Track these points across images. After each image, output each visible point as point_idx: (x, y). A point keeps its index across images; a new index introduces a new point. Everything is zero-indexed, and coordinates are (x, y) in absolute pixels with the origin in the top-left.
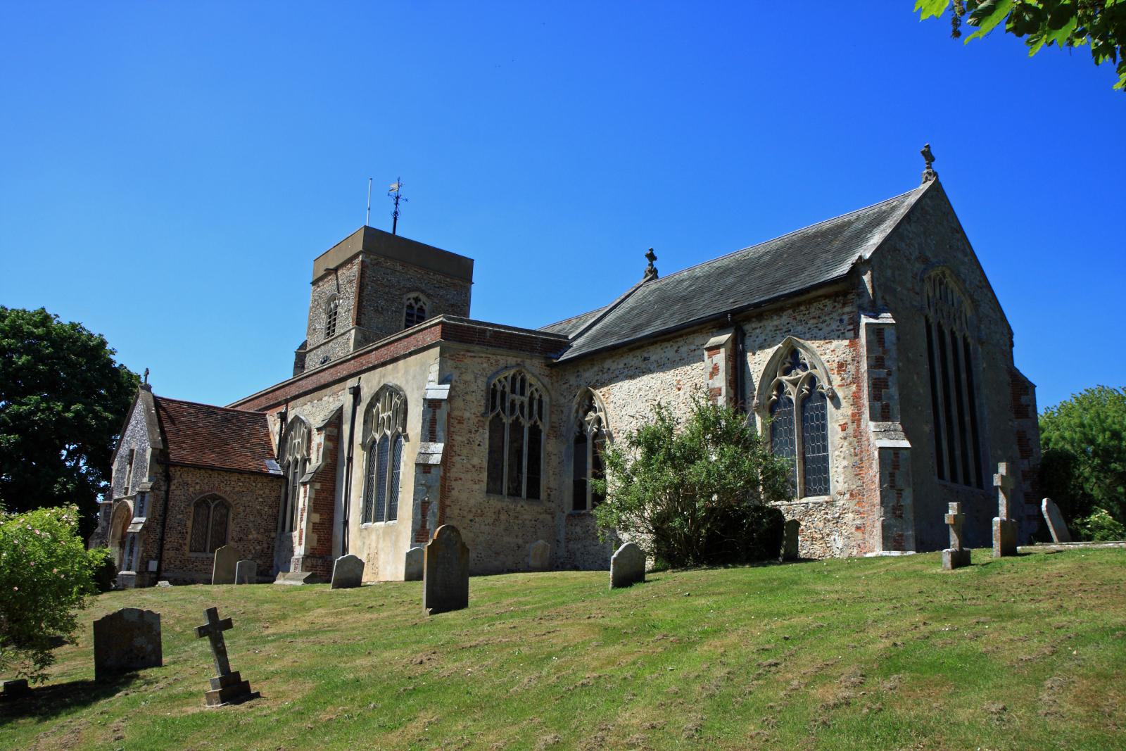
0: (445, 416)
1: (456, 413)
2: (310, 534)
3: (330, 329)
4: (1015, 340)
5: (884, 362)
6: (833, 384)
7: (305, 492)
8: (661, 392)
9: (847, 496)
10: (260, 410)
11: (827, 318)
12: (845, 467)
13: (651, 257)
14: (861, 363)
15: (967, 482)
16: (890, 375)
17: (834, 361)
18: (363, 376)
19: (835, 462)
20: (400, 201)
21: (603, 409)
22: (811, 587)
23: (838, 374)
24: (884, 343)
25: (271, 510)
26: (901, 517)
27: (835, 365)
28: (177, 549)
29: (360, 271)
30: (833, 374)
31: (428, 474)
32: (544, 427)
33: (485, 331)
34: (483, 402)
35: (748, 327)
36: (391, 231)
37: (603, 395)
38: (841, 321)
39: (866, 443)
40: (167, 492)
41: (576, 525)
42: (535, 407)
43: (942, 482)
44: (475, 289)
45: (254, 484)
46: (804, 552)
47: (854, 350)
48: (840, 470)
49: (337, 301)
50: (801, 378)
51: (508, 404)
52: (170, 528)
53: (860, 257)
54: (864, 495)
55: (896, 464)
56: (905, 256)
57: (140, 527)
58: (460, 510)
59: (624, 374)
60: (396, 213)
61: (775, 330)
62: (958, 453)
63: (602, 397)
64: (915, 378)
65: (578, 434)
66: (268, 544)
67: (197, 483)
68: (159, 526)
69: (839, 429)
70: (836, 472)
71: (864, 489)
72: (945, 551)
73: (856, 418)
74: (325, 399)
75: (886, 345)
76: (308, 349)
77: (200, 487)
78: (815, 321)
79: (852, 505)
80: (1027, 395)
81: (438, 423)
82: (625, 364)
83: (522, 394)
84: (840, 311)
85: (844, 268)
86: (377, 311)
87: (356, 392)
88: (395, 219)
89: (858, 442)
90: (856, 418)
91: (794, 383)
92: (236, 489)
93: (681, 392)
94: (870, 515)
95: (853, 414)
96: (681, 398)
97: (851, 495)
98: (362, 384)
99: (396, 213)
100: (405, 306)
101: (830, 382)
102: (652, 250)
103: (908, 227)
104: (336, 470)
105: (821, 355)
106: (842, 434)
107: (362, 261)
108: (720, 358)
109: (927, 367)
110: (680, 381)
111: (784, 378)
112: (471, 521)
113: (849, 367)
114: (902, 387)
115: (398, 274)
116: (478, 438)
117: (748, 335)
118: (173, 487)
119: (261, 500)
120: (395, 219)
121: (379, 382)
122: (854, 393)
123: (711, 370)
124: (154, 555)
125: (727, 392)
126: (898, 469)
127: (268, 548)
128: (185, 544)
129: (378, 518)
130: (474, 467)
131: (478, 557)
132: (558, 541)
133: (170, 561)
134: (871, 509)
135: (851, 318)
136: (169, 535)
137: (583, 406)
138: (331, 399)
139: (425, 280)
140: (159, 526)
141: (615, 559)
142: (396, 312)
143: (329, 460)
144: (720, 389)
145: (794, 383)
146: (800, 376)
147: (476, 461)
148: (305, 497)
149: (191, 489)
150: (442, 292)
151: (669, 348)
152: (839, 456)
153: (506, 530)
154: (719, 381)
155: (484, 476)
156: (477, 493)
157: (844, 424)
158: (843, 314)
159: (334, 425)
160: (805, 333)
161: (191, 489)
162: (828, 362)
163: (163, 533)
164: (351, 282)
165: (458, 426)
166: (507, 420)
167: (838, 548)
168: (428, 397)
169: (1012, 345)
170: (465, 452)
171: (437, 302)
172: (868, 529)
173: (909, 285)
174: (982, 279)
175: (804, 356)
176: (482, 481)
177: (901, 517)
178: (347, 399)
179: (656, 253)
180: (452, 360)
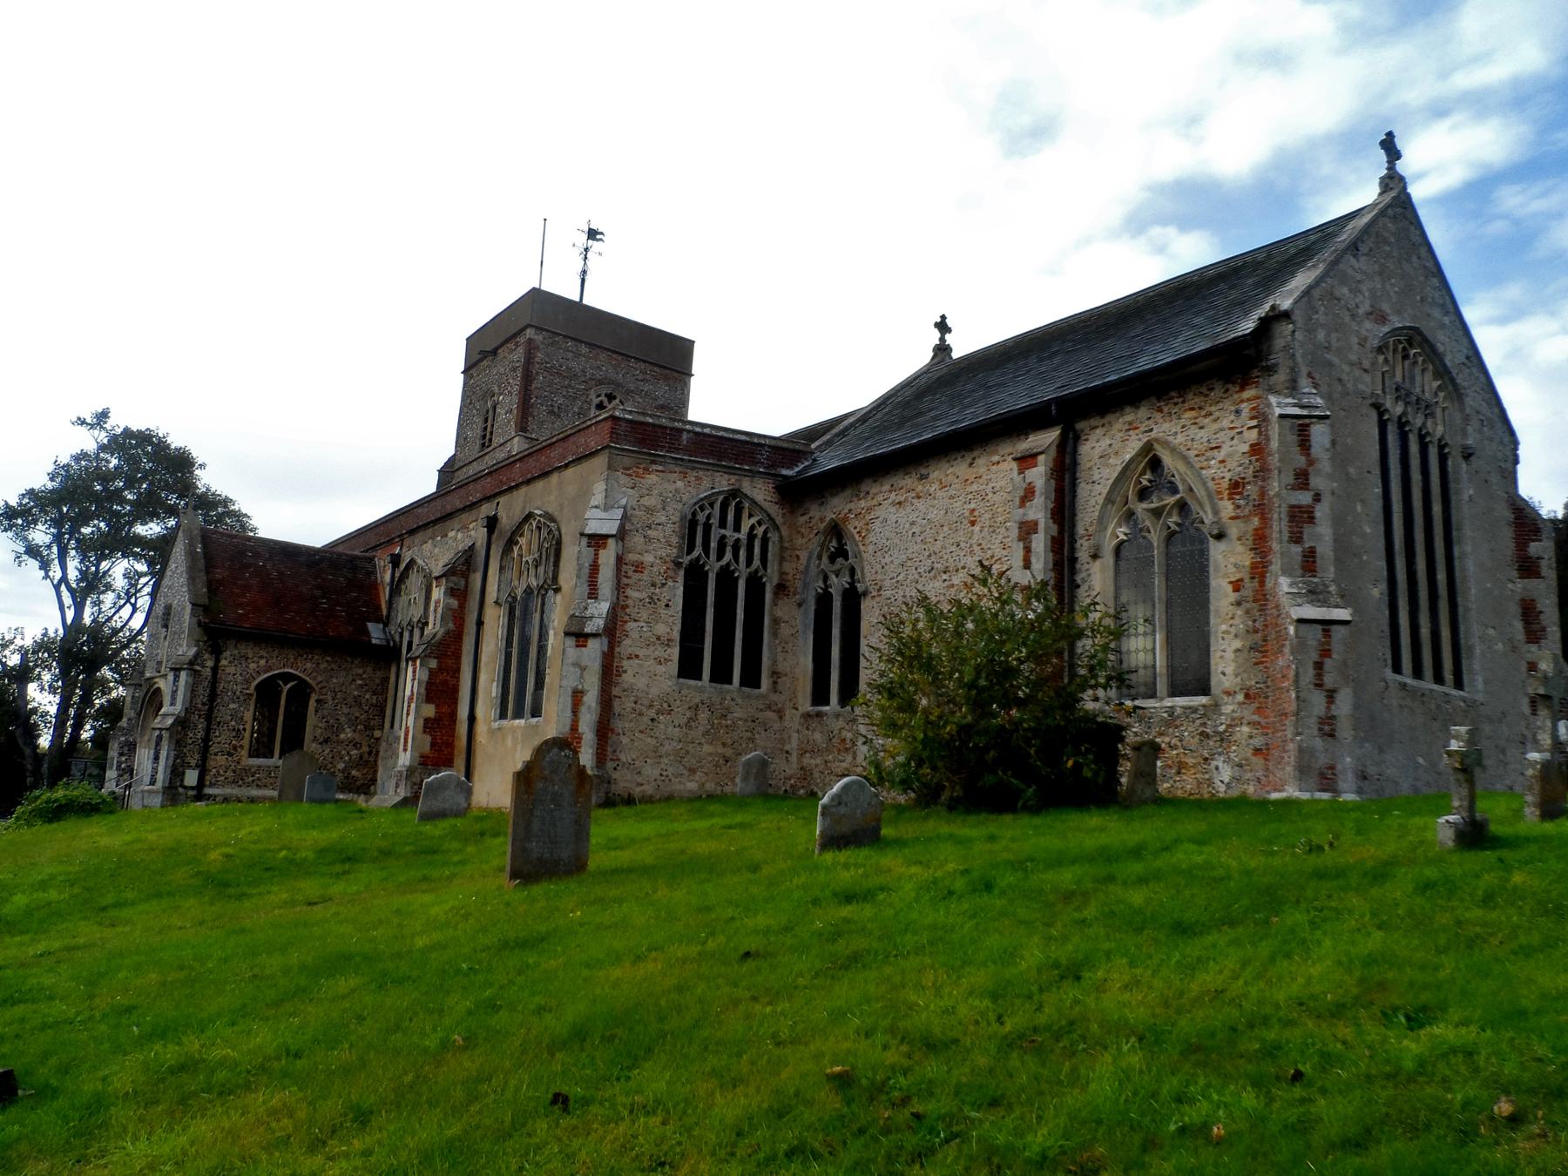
0: (612, 560)
1: (631, 557)
2: (419, 736)
4: (1521, 452)
5: (1307, 479)
6: (1222, 515)
7: (414, 672)
8: (945, 529)
9: (1240, 697)
10: (367, 551)
11: (1213, 409)
12: (1237, 650)
13: (942, 326)
14: (1270, 481)
15: (1439, 679)
16: (1319, 501)
17: (1223, 478)
18: (502, 500)
19: (1221, 641)
21: (857, 555)
23: (1229, 499)
24: (1309, 448)
25: (375, 697)
26: (1332, 735)
27: (1225, 484)
28: (230, 754)
30: (1222, 499)
31: (583, 649)
32: (771, 580)
34: (674, 540)
37: (859, 532)
38: (1238, 412)
39: (1275, 612)
40: (215, 669)
41: (814, 730)
42: (757, 550)
43: (1398, 677)
44: (694, 383)
46: (1166, 785)
47: (1257, 460)
48: (1230, 655)
49: (495, 398)
50: (1167, 505)
51: (713, 545)
52: (219, 723)
53: (1273, 308)
54: (1267, 697)
55: (1327, 647)
56: (1348, 309)
57: (170, 721)
58: (635, 703)
59: (890, 501)
60: (584, 272)
61: (1128, 430)
62: (1425, 631)
63: (857, 536)
64: (1359, 508)
65: (820, 591)
66: (370, 746)
67: (262, 657)
68: (202, 720)
69: (1230, 588)
70: (1221, 657)
71: (1268, 687)
72: (1442, 820)
73: (1259, 571)
74: (451, 534)
76: (456, 467)
77: (267, 662)
78: (1193, 414)
79: (1248, 713)
80: (1540, 540)
81: (601, 571)
83: (737, 528)
84: (1236, 396)
85: (1248, 326)
86: (551, 412)
87: (492, 523)
88: (583, 281)
89: (1261, 610)
90: (1259, 571)
91: (1157, 513)
93: (977, 528)
94: (1277, 731)
95: (1253, 563)
96: (976, 537)
97: (1247, 696)
99: (584, 272)
101: (1216, 512)
102: (943, 317)
103: (1353, 261)
104: (461, 639)
105: (1202, 468)
106: (1233, 597)
108: (1039, 474)
109: (1378, 490)
110: (973, 510)
111: (1141, 508)
112: (652, 720)
114: (1338, 521)
116: (664, 594)
118: (224, 662)
119: (359, 682)
120: (583, 281)
121: (524, 508)
122: (1256, 530)
124: (193, 763)
125: (1047, 529)
126: (1330, 656)
127: (370, 753)
128: (241, 747)
129: (518, 714)
130: (658, 639)
131: (661, 775)
132: (787, 752)
133: (218, 772)
134: (1281, 720)
135: (1253, 409)
136: (217, 734)
138: (460, 536)
140: (202, 720)
141: (825, 807)
143: (451, 626)
144: (1036, 523)
145: (1157, 513)
146: (1167, 502)
147: (661, 629)
148: (414, 680)
149: (253, 666)
152: (1226, 632)
153: (706, 733)
154: (1034, 509)
155: (675, 652)
156: (662, 679)
157: (1237, 581)
158: (1242, 401)
159: (463, 568)
160: (1176, 433)
162: (1213, 479)
163: (208, 730)
164: (514, 369)
165: (637, 576)
166: (713, 567)
167: (1222, 781)
168: (588, 531)
169: (1516, 461)
170: (644, 615)
171: (641, 400)
172: (1276, 753)
173: (1353, 357)
175: (1167, 460)
176: (671, 660)
177: (1332, 735)
178: (478, 534)
179: (949, 322)
180: (628, 475)
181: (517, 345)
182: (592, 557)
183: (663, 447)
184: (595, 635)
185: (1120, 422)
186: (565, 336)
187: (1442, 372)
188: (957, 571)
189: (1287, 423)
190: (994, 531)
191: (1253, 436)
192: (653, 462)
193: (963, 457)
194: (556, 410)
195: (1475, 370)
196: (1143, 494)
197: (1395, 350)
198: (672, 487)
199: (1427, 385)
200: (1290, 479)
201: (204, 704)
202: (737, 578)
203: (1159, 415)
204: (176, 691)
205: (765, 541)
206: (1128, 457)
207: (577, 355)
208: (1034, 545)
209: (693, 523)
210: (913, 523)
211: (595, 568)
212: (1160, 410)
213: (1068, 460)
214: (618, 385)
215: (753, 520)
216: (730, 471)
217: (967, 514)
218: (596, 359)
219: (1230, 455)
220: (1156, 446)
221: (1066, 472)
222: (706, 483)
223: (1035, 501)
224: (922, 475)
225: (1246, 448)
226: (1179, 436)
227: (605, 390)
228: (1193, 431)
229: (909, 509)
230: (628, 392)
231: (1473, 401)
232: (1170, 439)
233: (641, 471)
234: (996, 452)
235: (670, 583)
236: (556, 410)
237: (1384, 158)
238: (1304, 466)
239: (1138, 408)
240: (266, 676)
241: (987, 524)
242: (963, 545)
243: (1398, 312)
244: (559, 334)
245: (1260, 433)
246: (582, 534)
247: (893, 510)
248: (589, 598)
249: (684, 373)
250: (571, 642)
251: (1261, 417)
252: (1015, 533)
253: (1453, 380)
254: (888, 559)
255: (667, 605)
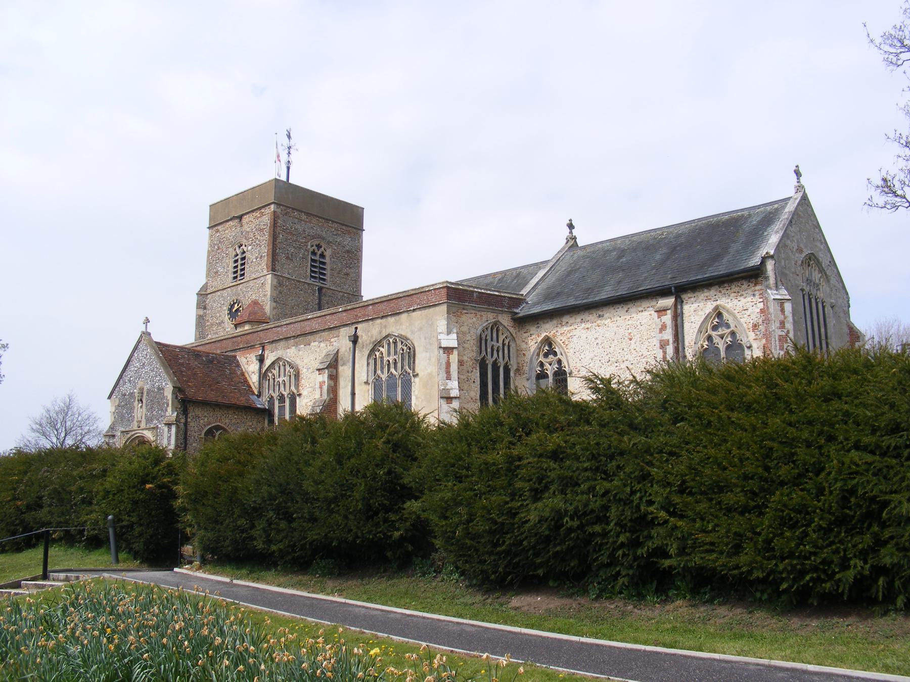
3: (239, 272)
11: (744, 293)
13: (571, 226)
18: (359, 326)
20: (292, 151)
22: (42, 673)
27: (751, 325)
29: (272, 220)
33: (473, 292)
35: (684, 297)
36: (285, 179)
44: (366, 236)
45: (245, 417)
51: (489, 350)
63: (562, 344)
67: (205, 416)
75: (786, 313)
76: (209, 291)
78: (735, 294)
82: (582, 319)
83: (498, 342)
84: (753, 288)
87: (355, 340)
88: (288, 168)
91: (722, 337)
92: (233, 421)
93: (633, 342)
98: (359, 333)
100: (310, 253)
102: (570, 220)
107: (274, 212)
108: (668, 318)
109: (804, 325)
111: (714, 334)
113: (760, 327)
115: (303, 222)
117: (685, 302)
121: (381, 332)
123: (660, 327)
137: (543, 350)
139: (325, 228)
142: (303, 258)
144: (668, 341)
145: (722, 337)
147: (472, 394)
149: (202, 421)
150: (339, 239)
151: (620, 308)
158: (755, 291)
161: (202, 421)
169: (849, 306)
173: (793, 270)
174: (831, 260)
175: (725, 314)
181: (262, 214)
182: (446, 359)
183: (467, 301)
184: (455, 398)
185: (702, 295)
186: (293, 209)
187: (822, 270)
188: (623, 362)
189: (776, 302)
190: (642, 343)
191: (761, 306)
192: (464, 309)
193: (623, 307)
194: (290, 256)
195: (833, 267)
196: (715, 328)
197: (806, 263)
198: (471, 321)
199: (816, 276)
200: (778, 325)
201: (181, 444)
202: (500, 366)
203: (720, 294)
204: (170, 437)
205: (509, 346)
206: (707, 312)
207: (300, 220)
208: (668, 350)
209: (481, 339)
210: (597, 338)
211: (448, 364)
212: (720, 292)
213: (679, 311)
214: (324, 239)
215: (504, 337)
216: (493, 311)
217: (627, 335)
218: (310, 222)
219: (752, 313)
220: (720, 308)
221: (678, 318)
222: (484, 319)
223: (667, 330)
224: (599, 315)
225: (759, 311)
226: (730, 304)
227: (316, 242)
228: (735, 302)
229: (593, 332)
230: (329, 243)
231: (833, 281)
232: (726, 305)
233: (459, 314)
234: (641, 306)
235: (474, 370)
236: (290, 256)
237: (796, 177)
238: (783, 319)
239: (710, 290)
240: (208, 427)
241: (639, 339)
242: (625, 349)
243: (806, 247)
244: (290, 208)
245: (764, 305)
246: (440, 347)
247: (584, 331)
248: (447, 379)
249: (360, 229)
250: (443, 402)
251: (765, 301)
252: (658, 345)
253: (825, 273)
254: (583, 356)
255: (474, 382)
